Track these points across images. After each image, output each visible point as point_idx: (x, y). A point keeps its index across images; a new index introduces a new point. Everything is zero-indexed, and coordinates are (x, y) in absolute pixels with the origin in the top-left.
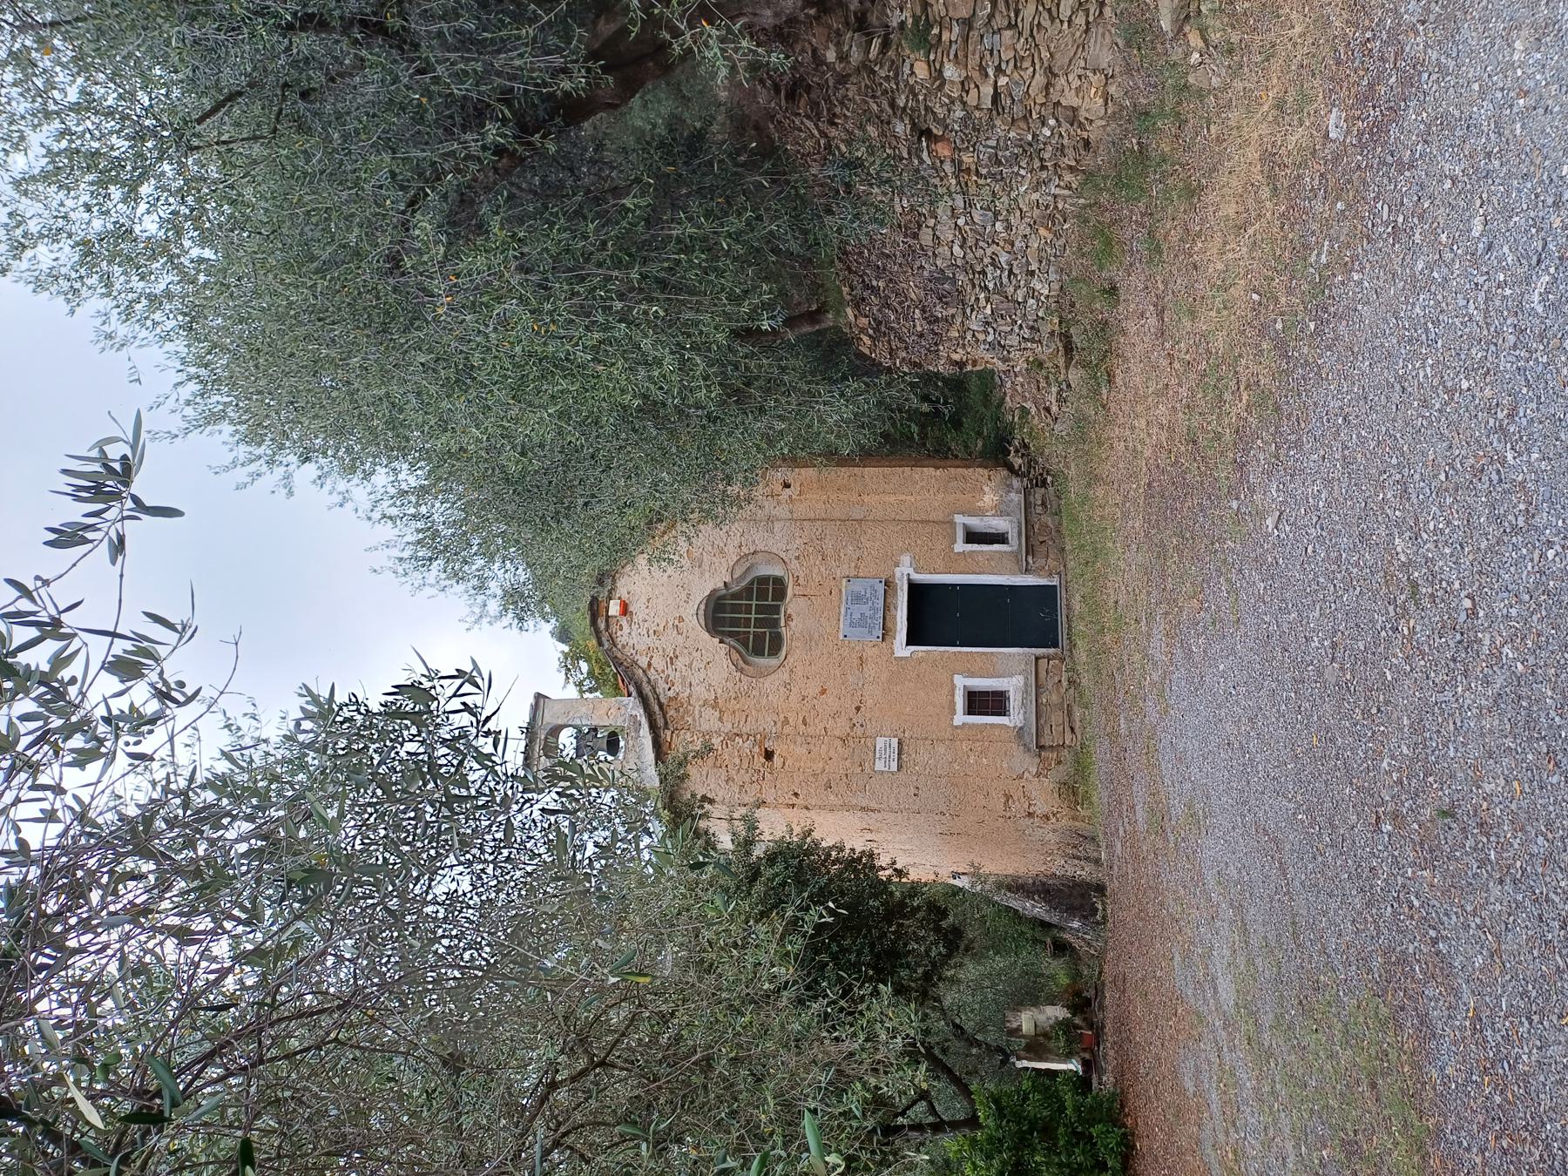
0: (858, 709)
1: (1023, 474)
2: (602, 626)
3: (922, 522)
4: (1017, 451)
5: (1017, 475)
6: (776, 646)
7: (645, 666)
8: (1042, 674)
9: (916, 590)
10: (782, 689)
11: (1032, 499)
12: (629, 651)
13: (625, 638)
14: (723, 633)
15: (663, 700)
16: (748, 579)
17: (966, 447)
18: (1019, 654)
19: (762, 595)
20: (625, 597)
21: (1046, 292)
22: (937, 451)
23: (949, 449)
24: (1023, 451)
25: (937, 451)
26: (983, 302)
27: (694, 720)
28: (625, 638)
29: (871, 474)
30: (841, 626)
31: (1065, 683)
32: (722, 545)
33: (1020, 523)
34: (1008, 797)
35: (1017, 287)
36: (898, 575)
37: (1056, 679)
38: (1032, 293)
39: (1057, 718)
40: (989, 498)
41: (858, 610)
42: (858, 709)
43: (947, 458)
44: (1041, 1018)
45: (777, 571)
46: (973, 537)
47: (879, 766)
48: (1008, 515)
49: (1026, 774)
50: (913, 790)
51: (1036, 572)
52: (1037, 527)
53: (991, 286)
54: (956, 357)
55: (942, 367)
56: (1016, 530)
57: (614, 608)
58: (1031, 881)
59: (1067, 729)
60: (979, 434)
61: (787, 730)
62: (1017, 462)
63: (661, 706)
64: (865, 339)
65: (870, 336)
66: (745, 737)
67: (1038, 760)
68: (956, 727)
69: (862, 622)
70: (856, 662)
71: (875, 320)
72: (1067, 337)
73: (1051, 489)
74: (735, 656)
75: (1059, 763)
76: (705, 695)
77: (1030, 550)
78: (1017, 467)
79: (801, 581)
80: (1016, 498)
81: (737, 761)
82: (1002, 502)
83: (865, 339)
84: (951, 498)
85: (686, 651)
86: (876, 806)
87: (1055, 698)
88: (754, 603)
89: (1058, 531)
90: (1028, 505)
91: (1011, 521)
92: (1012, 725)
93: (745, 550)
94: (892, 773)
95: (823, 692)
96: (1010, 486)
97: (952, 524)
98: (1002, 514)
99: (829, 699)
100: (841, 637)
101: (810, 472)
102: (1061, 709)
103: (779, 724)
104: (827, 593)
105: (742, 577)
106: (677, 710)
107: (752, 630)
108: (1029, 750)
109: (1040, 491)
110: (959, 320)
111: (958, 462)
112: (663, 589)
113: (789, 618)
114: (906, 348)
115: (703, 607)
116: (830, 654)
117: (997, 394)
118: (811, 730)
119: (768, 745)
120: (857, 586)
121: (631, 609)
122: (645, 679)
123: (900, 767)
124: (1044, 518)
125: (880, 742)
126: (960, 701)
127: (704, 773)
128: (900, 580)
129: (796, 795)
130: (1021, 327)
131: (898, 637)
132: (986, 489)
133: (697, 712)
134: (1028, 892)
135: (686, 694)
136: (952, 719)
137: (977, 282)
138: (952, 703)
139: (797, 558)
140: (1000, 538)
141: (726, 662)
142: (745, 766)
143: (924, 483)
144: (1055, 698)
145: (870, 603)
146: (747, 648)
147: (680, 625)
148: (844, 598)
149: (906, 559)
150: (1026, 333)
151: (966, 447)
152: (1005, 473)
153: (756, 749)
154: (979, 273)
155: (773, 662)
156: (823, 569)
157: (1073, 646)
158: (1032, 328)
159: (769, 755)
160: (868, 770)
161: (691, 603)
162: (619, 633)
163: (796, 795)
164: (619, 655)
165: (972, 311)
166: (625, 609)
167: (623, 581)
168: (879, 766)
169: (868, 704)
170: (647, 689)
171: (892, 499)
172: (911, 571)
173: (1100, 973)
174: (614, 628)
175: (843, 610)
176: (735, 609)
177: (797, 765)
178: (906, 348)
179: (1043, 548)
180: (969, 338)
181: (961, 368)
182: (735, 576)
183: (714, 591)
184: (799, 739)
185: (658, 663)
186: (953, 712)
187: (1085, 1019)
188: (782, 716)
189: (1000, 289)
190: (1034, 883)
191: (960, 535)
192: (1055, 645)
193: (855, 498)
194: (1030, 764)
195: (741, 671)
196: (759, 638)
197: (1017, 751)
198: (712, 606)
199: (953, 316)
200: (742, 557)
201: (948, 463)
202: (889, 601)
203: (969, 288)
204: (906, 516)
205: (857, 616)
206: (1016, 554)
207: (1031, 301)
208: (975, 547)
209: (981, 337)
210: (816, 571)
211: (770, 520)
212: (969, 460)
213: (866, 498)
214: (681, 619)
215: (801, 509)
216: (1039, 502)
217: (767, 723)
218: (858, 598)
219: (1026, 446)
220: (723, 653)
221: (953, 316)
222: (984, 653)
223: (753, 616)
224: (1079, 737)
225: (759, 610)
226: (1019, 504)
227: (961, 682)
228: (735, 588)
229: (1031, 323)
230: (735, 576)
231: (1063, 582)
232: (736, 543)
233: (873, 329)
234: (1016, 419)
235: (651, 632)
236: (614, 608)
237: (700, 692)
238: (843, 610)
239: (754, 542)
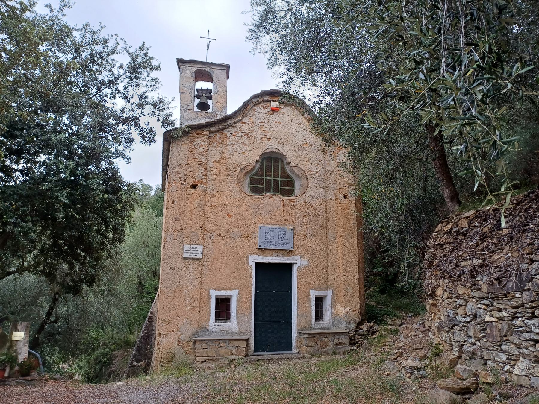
0: (220, 235)
1: (358, 331)
2: (265, 98)
3: (327, 271)
4: (371, 327)
5: (357, 327)
6: (256, 190)
7: (244, 121)
8: (237, 343)
9: (288, 267)
10: (231, 193)
11: (342, 336)
12: (252, 112)
13: (259, 111)
14: (263, 161)
15: (225, 131)
16: (293, 176)
17: (371, 296)
18: (250, 329)
19: (284, 183)
20: (281, 111)
21: (515, 372)
22: (368, 281)
23: (369, 288)
24: (371, 331)
25: (368, 281)
26: (499, 314)
27: (215, 147)
28: (259, 111)
29: (354, 243)
30: (266, 226)
31: (231, 357)
32: (311, 161)
33: (328, 329)
34: (168, 322)
35: (519, 346)
36: (296, 257)
37: (234, 352)
38: (512, 359)
39: (211, 352)
40: (342, 310)
41: (275, 235)
42: (220, 235)
43: (365, 286)
44: (21, 344)
45: (297, 191)
46: (319, 301)
47: (186, 247)
48: (333, 322)
49: (179, 333)
50: (173, 267)
51: (299, 339)
52: (326, 339)
53: (517, 322)
54: (439, 292)
55: (429, 281)
56: (324, 326)
57: (274, 104)
58: (154, 328)
59: (204, 358)
60: (378, 303)
61: (208, 197)
62: (364, 328)
63: (222, 130)
64: (449, 226)
65: (452, 229)
66: (204, 174)
67: (188, 339)
68: (209, 291)
69: (269, 237)
70: (246, 234)
71: (467, 231)
72: (476, 389)
73: (349, 348)
74: (249, 168)
75: (186, 353)
76: (228, 153)
77: (312, 336)
78: (361, 327)
79: (291, 204)
80: (343, 327)
81: (190, 170)
82: (340, 317)
83: (449, 226)
84: (342, 288)
85: (252, 142)
86: (166, 246)
87: (223, 351)
88: (280, 179)
89: (324, 352)
90: (339, 334)
91: (329, 324)
92: (210, 324)
93: (308, 174)
94: (182, 255)
95: (229, 216)
96: (350, 323)
97: (327, 289)
98: (335, 317)
99: (225, 219)
100: (260, 226)
101: (353, 207)
102: (217, 355)
103: (212, 192)
104: (285, 218)
105: (293, 172)
106: (220, 138)
107: (264, 178)
108: (194, 335)
109: (347, 341)
110: (477, 294)
111: (363, 292)
112: (286, 130)
113: (271, 197)
114: (445, 255)
115: (276, 151)
116: (250, 220)
117: (402, 314)
118: (208, 209)
119: (200, 187)
120: (289, 235)
121: (275, 114)
122: (236, 120)
123: (185, 259)
124: (331, 344)
125: (200, 248)
126: (223, 293)
127: (185, 152)
128: (293, 259)
129: (173, 202)
130: (473, 344)
131: (260, 257)
132: (348, 309)
133: (219, 148)
134: (149, 327)
135: (229, 143)
136: (213, 289)
137: (520, 310)
138: (221, 289)
139: (304, 202)
140: (319, 316)
141: (246, 163)
142: (189, 174)
143: (349, 272)
144: (223, 351)
145: (280, 242)
146: (254, 175)
147: (266, 139)
148: (282, 227)
149: (305, 262)
150: (470, 348)
151: (371, 296)
152: (358, 320)
153: (197, 180)
154: (533, 313)
155: (247, 189)
156: (298, 215)
157: (253, 363)
158: (473, 353)
159: (194, 187)
160: (184, 241)
161: (278, 145)
162: (262, 107)
163: (173, 202)
164: (249, 107)
165: (487, 305)
166: (274, 110)
167: (290, 110)
168: (186, 247)
169: (222, 241)
170: (231, 122)
171: (340, 254)
172: (298, 265)
173: (55, 379)
174: (264, 105)
175: (274, 226)
176: (276, 170)
177: (188, 202)
178: (445, 255)
179: (313, 344)
180: (458, 302)
181: (430, 295)
182: (294, 168)
183: (285, 157)
184: (203, 202)
185: (246, 128)
186: (217, 290)
187: (15, 373)
188: (216, 194)
189: (512, 330)
190: (152, 330)
191: (320, 293)
192: (255, 351)
193: (340, 233)
194: (185, 336)
195: (241, 172)
196: (260, 182)
197: (194, 327)
198: (278, 156)
199: (479, 290)
200: (304, 172)
201: (362, 287)
202: (281, 252)
203: (513, 303)
204: (330, 261)
205: (272, 234)
206: (309, 327)
207: (504, 357)
208: (313, 302)
209: (460, 311)
210: (298, 212)
211: (326, 188)
212: (364, 298)
213: (340, 240)
214: (269, 140)
215: (332, 205)
216: (341, 341)
217: (212, 185)
218: (282, 235)
219: (373, 333)
220: (251, 162)
221: (479, 290)
222: (251, 307)
223: (272, 178)
224: (199, 366)
225: (276, 182)
226: (340, 328)
227: (234, 294)
228: (287, 168)
229: (479, 353)
230: (294, 168)
231: (293, 356)
232: (312, 169)
233: (458, 231)
234: (390, 327)
235: (262, 124)
236: (274, 104)
237: (230, 150)
238: (274, 226)
239: (313, 178)
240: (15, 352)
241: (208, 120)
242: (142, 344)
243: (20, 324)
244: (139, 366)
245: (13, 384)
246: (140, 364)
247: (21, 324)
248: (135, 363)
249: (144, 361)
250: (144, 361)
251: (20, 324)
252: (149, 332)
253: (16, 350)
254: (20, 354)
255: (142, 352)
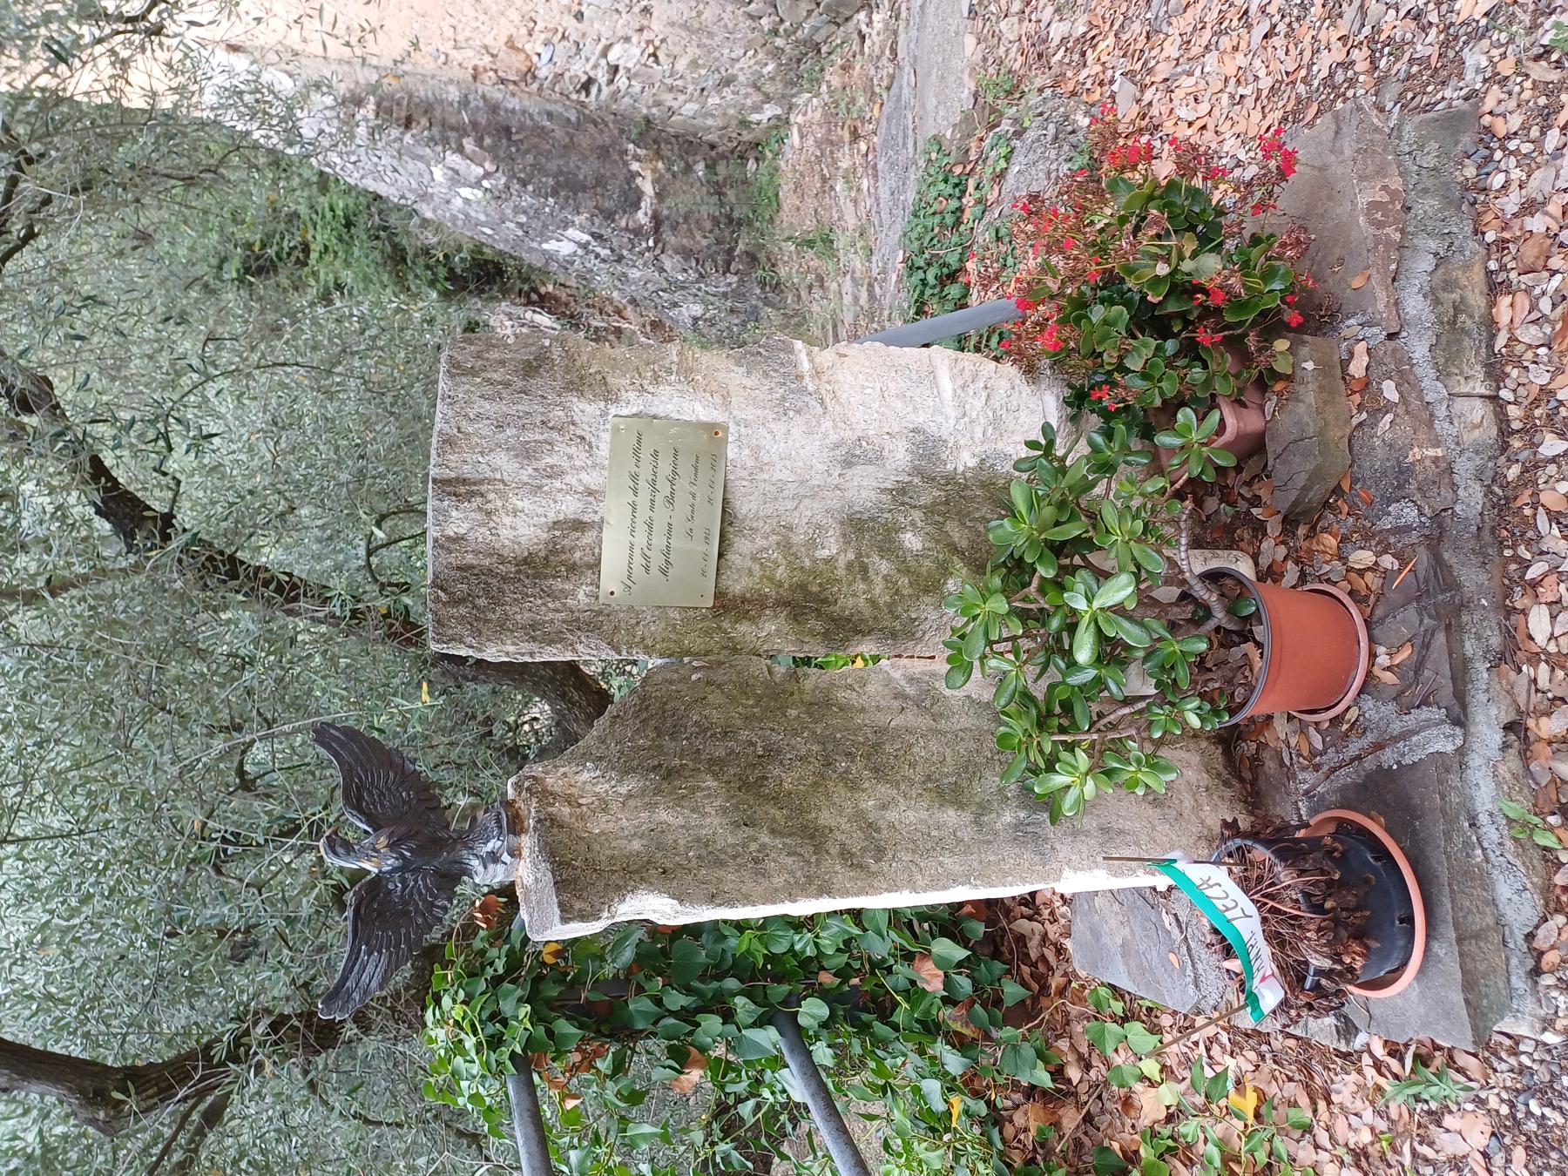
190: (465, 102)
240: (888, 544)
241: (76, 1052)
242: (543, 171)
243: (459, 520)
244: (660, 196)
245: (1478, 411)
246: (648, 188)
247: (459, 489)
248: (642, 217)
249: (635, 166)
250: (635, 166)
251: (459, 520)
252: (474, 124)
253: (856, 525)
254: (927, 448)
255: (586, 171)
